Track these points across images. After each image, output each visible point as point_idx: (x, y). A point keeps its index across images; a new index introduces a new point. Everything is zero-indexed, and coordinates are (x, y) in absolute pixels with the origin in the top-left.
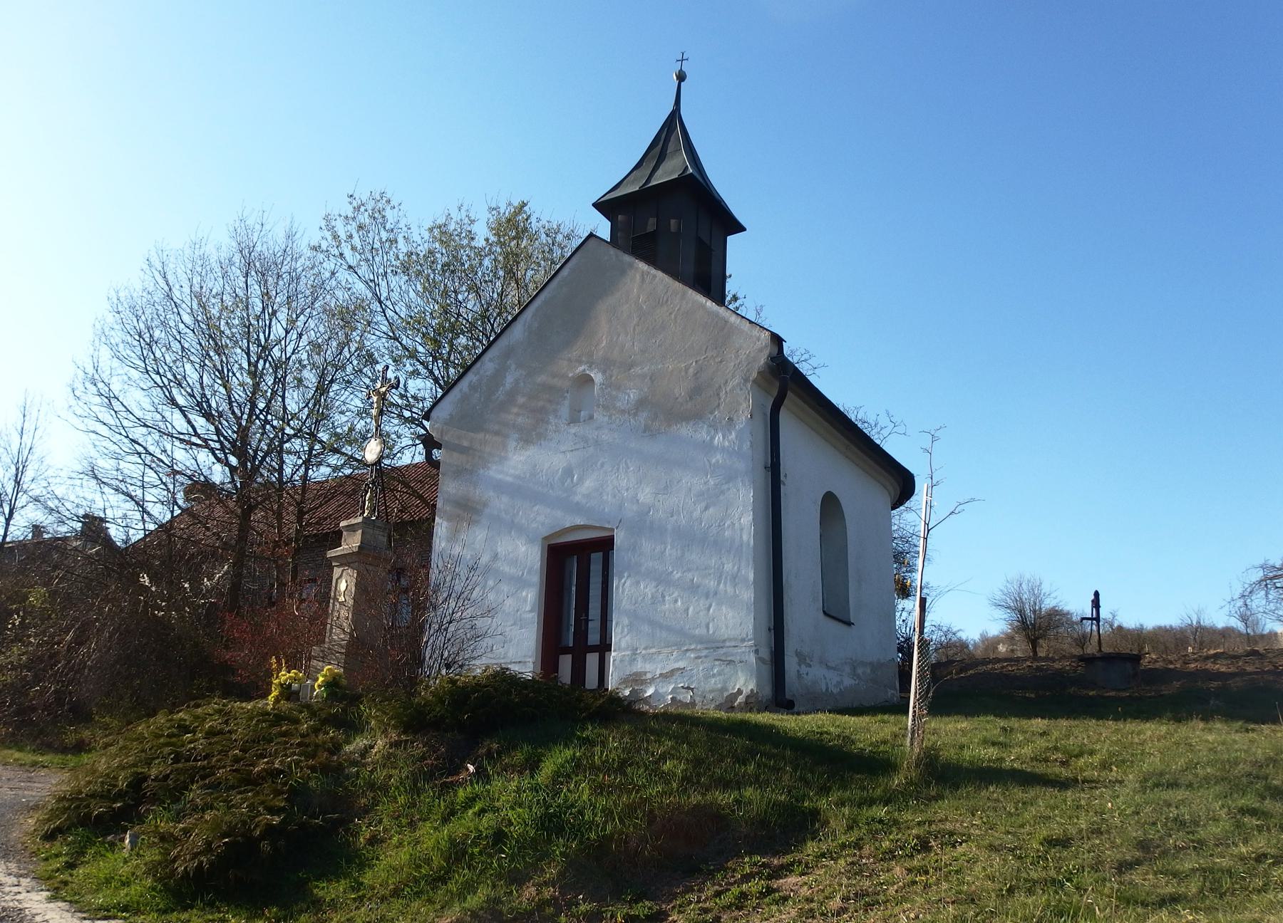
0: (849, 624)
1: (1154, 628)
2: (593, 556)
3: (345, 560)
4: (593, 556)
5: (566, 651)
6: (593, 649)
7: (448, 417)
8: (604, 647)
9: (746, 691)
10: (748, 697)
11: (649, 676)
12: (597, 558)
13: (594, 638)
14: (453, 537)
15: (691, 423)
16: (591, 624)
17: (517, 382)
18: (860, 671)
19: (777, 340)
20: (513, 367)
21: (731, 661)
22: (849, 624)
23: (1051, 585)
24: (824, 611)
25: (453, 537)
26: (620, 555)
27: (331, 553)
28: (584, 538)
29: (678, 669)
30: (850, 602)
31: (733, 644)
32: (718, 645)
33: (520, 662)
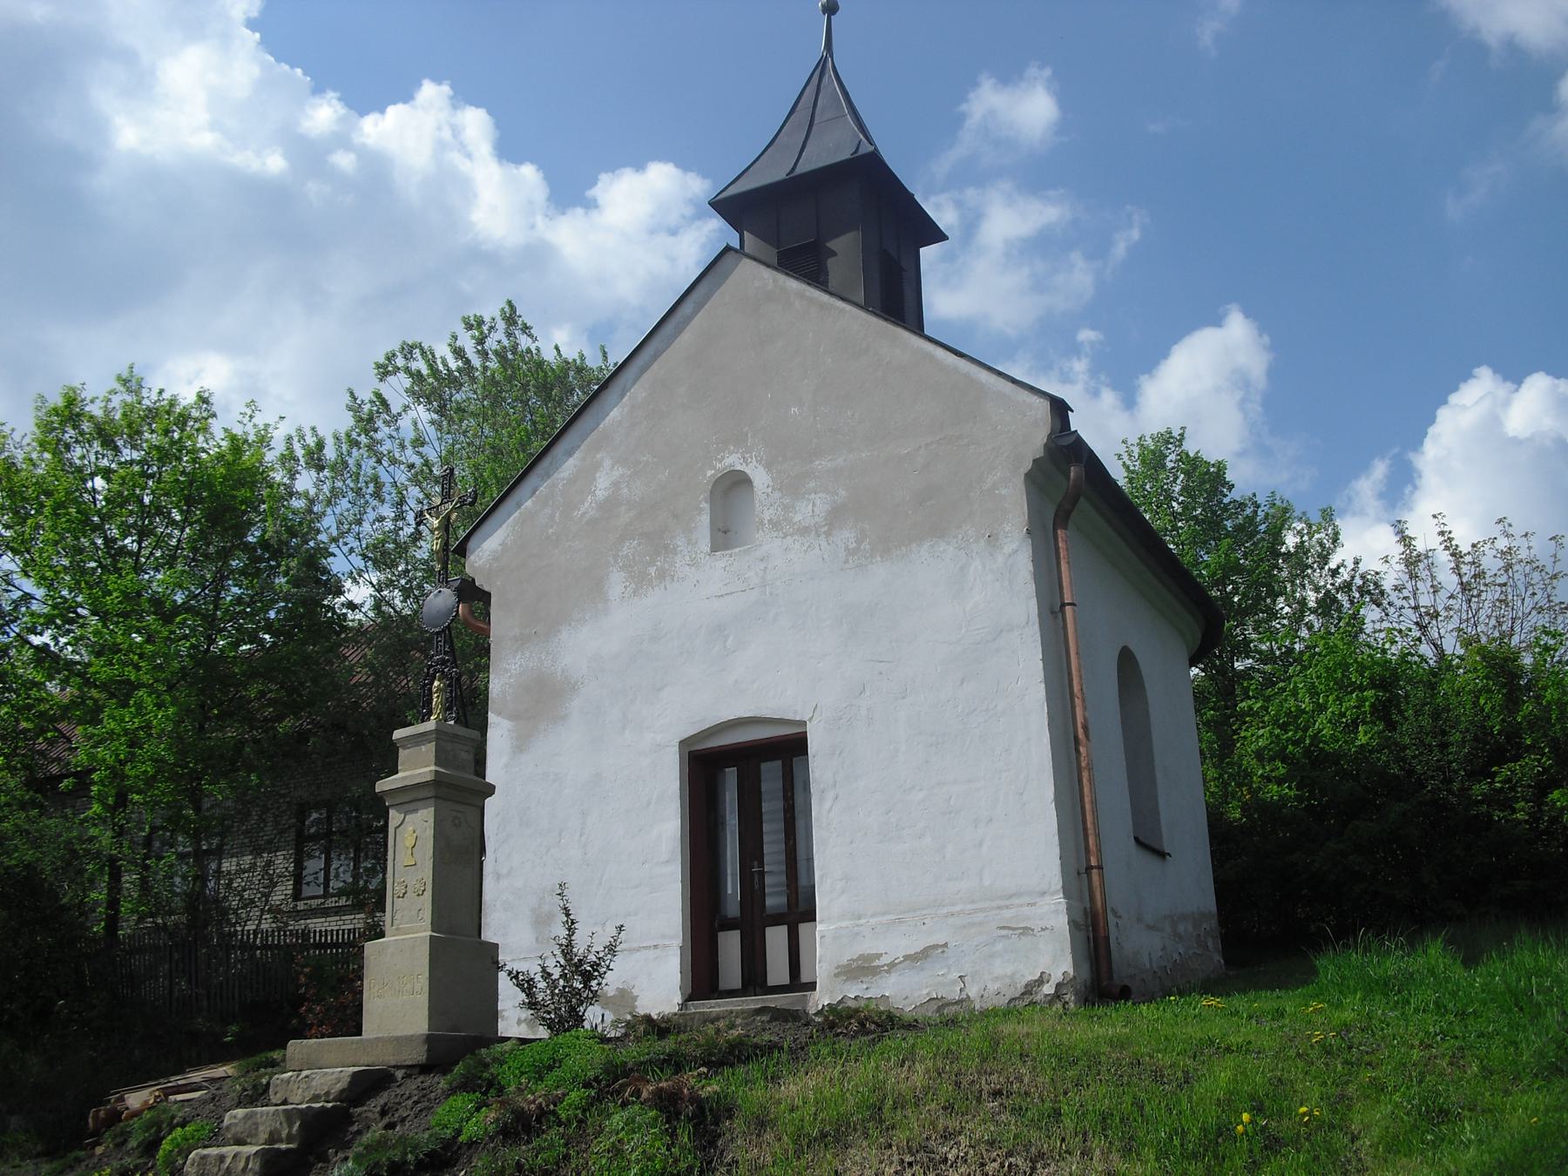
0: (1162, 855)
1: (438, 612)
2: (765, 766)
3: (412, 796)
4: (765, 766)
5: (729, 925)
6: (776, 920)
7: (499, 548)
8: (801, 910)
9: (1057, 977)
10: (1059, 986)
11: (885, 960)
12: (771, 772)
13: (775, 900)
14: (521, 745)
15: (926, 545)
16: (768, 880)
17: (616, 485)
18: (1181, 928)
19: (1060, 409)
20: (607, 463)
21: (1026, 928)
22: (1162, 855)
23: (666, 588)
24: (1136, 839)
25: (521, 745)
26: (820, 765)
27: (382, 785)
28: (740, 740)
29: (935, 947)
30: (1162, 821)
31: (1026, 899)
32: (1001, 903)
33: (656, 947)
